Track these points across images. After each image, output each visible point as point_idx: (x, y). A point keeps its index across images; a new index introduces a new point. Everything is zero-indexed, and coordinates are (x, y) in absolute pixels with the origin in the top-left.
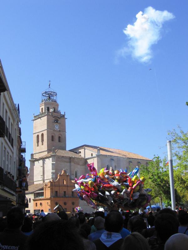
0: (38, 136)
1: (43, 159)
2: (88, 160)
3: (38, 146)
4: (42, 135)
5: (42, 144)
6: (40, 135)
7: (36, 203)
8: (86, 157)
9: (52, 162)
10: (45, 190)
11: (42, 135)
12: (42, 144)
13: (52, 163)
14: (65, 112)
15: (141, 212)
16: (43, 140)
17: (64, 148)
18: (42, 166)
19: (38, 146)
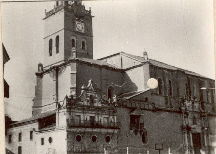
0: (51, 41)
1: (57, 70)
2: (128, 72)
3: (51, 55)
4: (58, 38)
5: (57, 52)
6: (54, 39)
7: (43, 139)
8: (124, 67)
9: (71, 71)
10: (58, 113)
11: (58, 38)
12: (57, 52)
13: (72, 72)
14: (90, 8)
15: (191, 122)
16: (57, 45)
17: (91, 57)
18: (55, 93)
19: (51, 55)
